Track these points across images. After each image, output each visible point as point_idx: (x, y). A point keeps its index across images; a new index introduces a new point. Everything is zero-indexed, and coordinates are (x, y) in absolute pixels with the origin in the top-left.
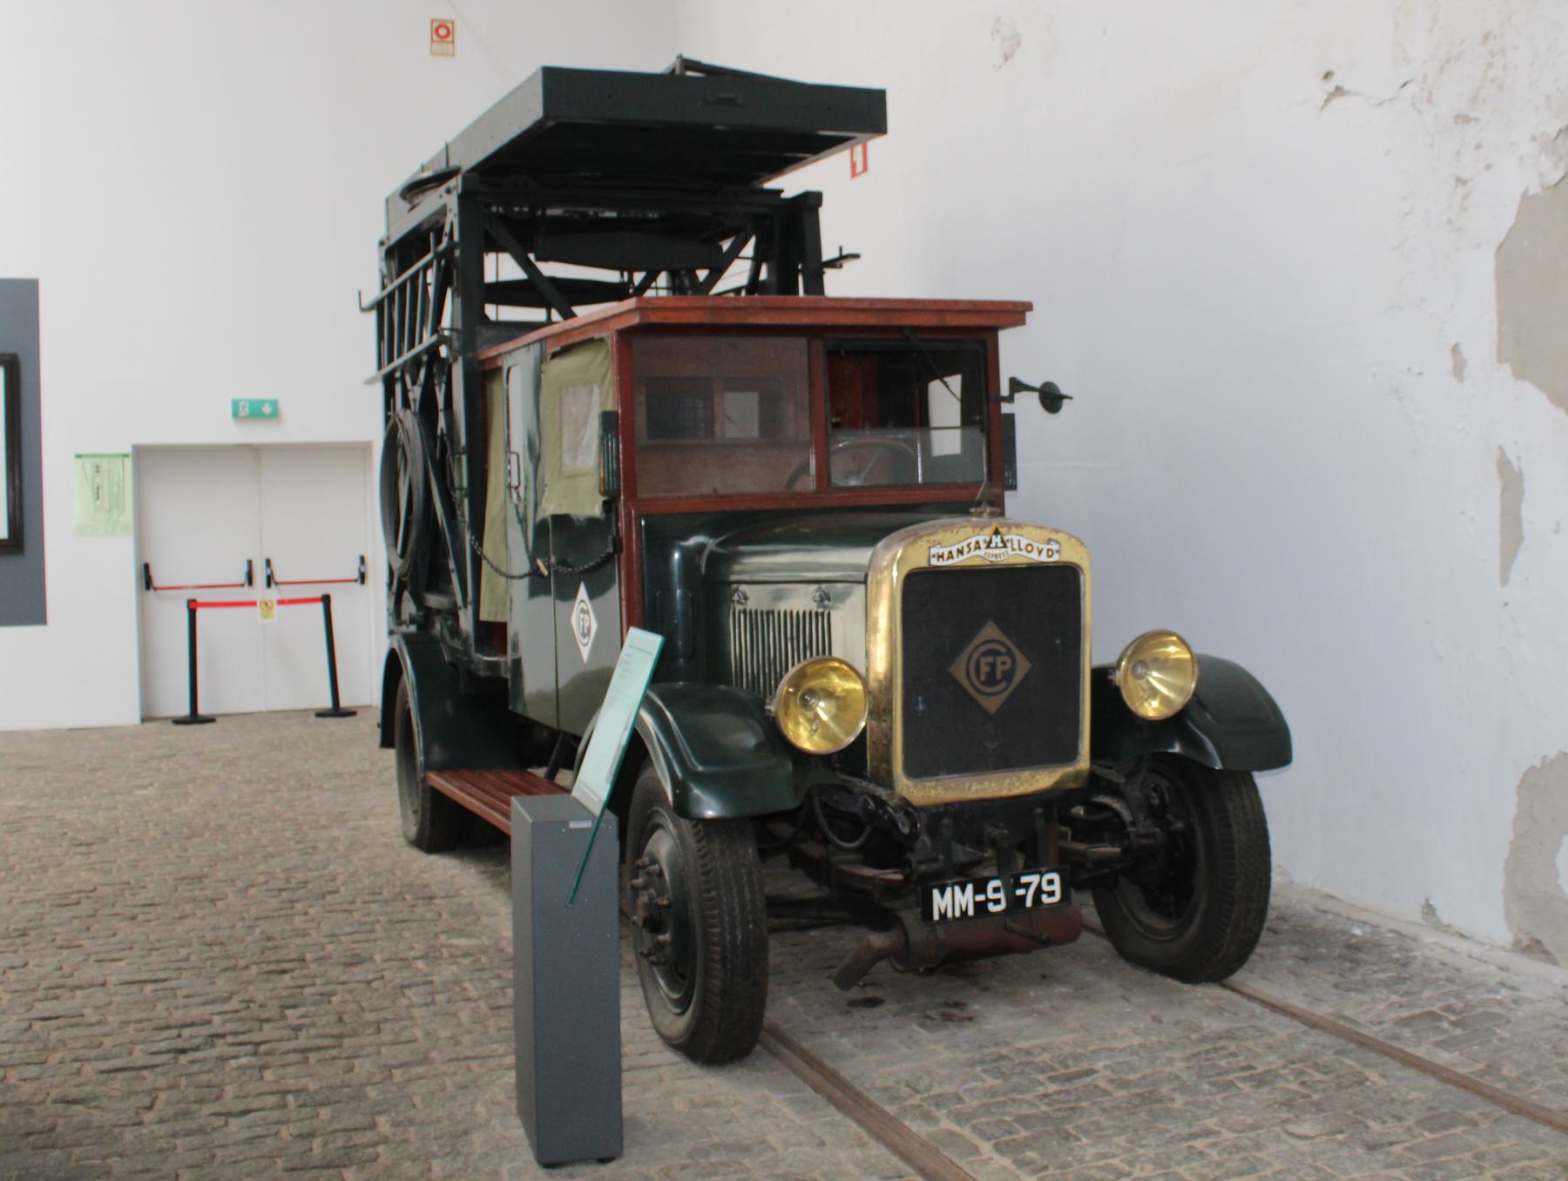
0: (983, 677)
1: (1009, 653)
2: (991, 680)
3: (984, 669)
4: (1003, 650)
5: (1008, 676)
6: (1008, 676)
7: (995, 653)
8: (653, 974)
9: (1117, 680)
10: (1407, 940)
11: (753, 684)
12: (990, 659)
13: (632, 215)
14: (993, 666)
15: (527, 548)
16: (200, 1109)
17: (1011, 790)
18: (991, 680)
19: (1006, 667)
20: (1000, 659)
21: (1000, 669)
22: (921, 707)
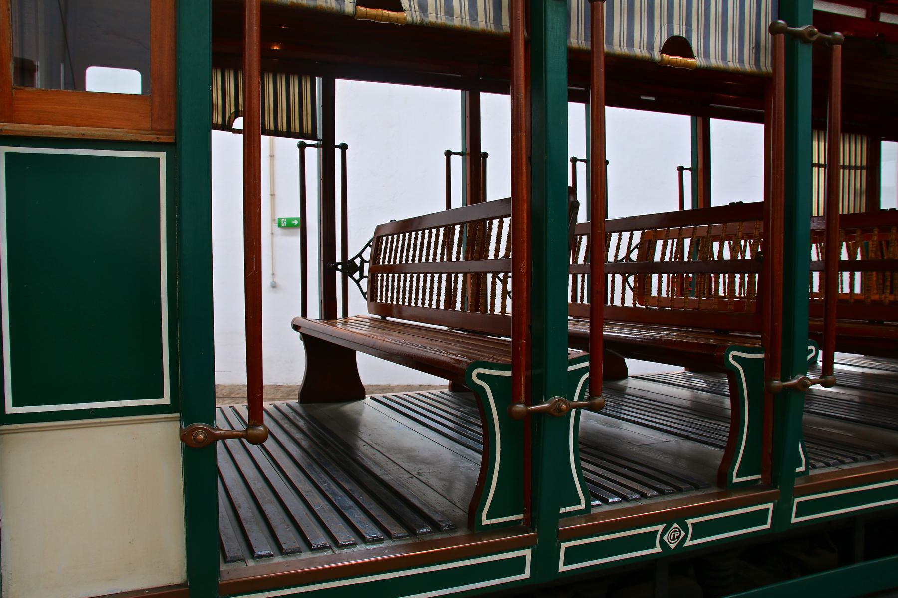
0: (671, 539)
1: (680, 531)
2: (674, 539)
3: (672, 536)
4: (678, 530)
5: (678, 537)
6: (678, 537)
8: (469, 358)
9: (335, 8)
10: (232, 112)
11: (714, 385)
12: (674, 533)
13: (586, 394)
14: (674, 535)
15: (660, 47)
16: (276, 223)
17: (247, 523)
18: (674, 539)
19: (678, 535)
20: (676, 533)
21: (676, 535)
22: (685, 275)
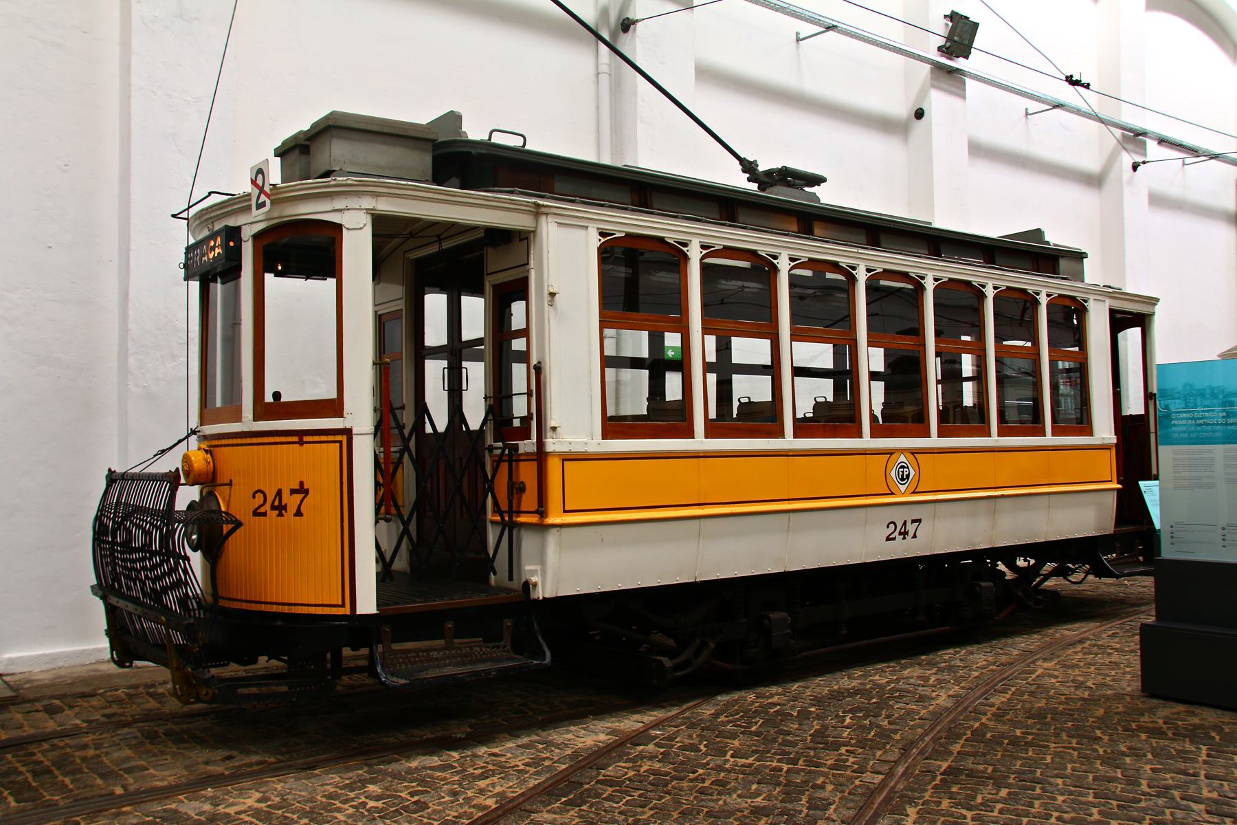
1: (908, 467)
5: (908, 476)
7: (902, 467)
14: (903, 472)
18: (902, 479)
19: (907, 473)
20: (905, 470)
21: (905, 473)
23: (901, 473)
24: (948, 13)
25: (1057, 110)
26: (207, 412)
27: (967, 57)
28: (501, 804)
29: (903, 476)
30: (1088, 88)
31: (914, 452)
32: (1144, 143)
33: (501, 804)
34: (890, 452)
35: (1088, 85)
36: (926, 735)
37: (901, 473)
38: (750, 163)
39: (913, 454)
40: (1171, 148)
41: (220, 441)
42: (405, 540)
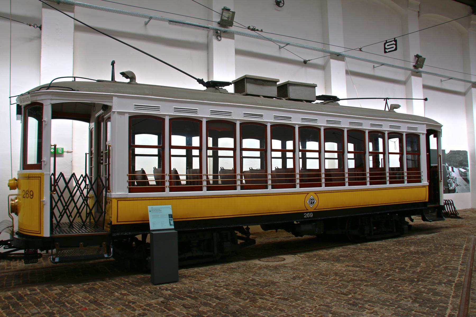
5: (314, 202)
14: (312, 201)
18: (311, 203)
23: (311, 202)
24: (416, 55)
25: (382, 66)
26: (130, 173)
27: (422, 68)
28: (175, 298)
29: (311, 202)
30: (262, 32)
31: (316, 193)
32: (421, 75)
33: (175, 298)
34: (307, 193)
35: (262, 30)
36: (321, 310)
37: (311, 202)
38: (201, 80)
39: (315, 193)
40: (427, 74)
41: (443, 305)
42: (82, 177)
